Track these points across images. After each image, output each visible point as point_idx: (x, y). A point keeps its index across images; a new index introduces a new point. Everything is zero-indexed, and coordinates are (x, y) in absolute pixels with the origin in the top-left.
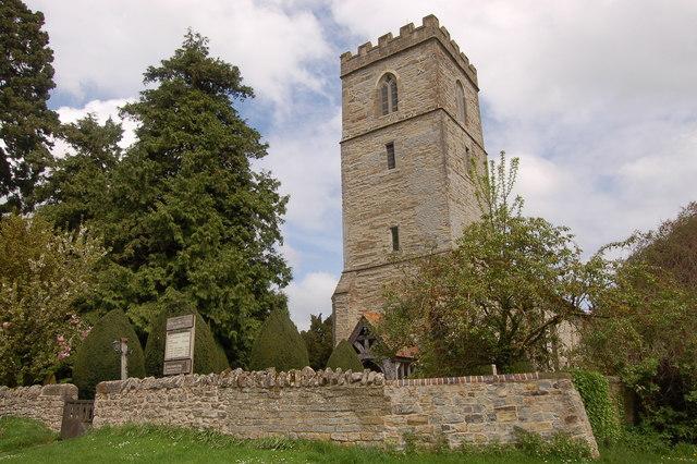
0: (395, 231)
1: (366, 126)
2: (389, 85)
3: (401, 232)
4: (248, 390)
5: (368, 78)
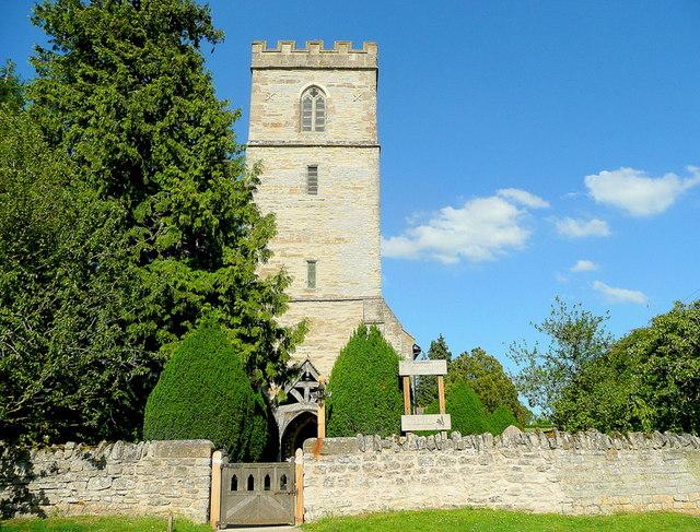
0: (311, 262)
1: (290, 135)
2: (314, 100)
3: (318, 267)
4: (583, 452)
5: (288, 81)
